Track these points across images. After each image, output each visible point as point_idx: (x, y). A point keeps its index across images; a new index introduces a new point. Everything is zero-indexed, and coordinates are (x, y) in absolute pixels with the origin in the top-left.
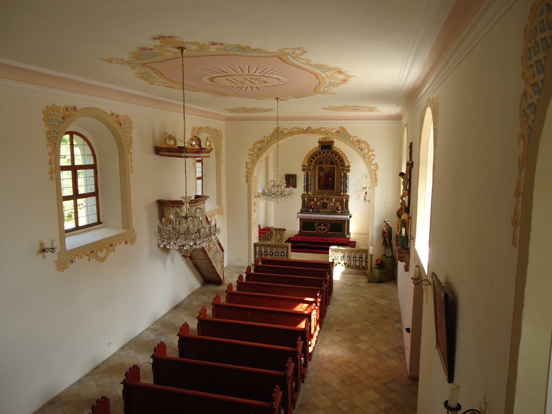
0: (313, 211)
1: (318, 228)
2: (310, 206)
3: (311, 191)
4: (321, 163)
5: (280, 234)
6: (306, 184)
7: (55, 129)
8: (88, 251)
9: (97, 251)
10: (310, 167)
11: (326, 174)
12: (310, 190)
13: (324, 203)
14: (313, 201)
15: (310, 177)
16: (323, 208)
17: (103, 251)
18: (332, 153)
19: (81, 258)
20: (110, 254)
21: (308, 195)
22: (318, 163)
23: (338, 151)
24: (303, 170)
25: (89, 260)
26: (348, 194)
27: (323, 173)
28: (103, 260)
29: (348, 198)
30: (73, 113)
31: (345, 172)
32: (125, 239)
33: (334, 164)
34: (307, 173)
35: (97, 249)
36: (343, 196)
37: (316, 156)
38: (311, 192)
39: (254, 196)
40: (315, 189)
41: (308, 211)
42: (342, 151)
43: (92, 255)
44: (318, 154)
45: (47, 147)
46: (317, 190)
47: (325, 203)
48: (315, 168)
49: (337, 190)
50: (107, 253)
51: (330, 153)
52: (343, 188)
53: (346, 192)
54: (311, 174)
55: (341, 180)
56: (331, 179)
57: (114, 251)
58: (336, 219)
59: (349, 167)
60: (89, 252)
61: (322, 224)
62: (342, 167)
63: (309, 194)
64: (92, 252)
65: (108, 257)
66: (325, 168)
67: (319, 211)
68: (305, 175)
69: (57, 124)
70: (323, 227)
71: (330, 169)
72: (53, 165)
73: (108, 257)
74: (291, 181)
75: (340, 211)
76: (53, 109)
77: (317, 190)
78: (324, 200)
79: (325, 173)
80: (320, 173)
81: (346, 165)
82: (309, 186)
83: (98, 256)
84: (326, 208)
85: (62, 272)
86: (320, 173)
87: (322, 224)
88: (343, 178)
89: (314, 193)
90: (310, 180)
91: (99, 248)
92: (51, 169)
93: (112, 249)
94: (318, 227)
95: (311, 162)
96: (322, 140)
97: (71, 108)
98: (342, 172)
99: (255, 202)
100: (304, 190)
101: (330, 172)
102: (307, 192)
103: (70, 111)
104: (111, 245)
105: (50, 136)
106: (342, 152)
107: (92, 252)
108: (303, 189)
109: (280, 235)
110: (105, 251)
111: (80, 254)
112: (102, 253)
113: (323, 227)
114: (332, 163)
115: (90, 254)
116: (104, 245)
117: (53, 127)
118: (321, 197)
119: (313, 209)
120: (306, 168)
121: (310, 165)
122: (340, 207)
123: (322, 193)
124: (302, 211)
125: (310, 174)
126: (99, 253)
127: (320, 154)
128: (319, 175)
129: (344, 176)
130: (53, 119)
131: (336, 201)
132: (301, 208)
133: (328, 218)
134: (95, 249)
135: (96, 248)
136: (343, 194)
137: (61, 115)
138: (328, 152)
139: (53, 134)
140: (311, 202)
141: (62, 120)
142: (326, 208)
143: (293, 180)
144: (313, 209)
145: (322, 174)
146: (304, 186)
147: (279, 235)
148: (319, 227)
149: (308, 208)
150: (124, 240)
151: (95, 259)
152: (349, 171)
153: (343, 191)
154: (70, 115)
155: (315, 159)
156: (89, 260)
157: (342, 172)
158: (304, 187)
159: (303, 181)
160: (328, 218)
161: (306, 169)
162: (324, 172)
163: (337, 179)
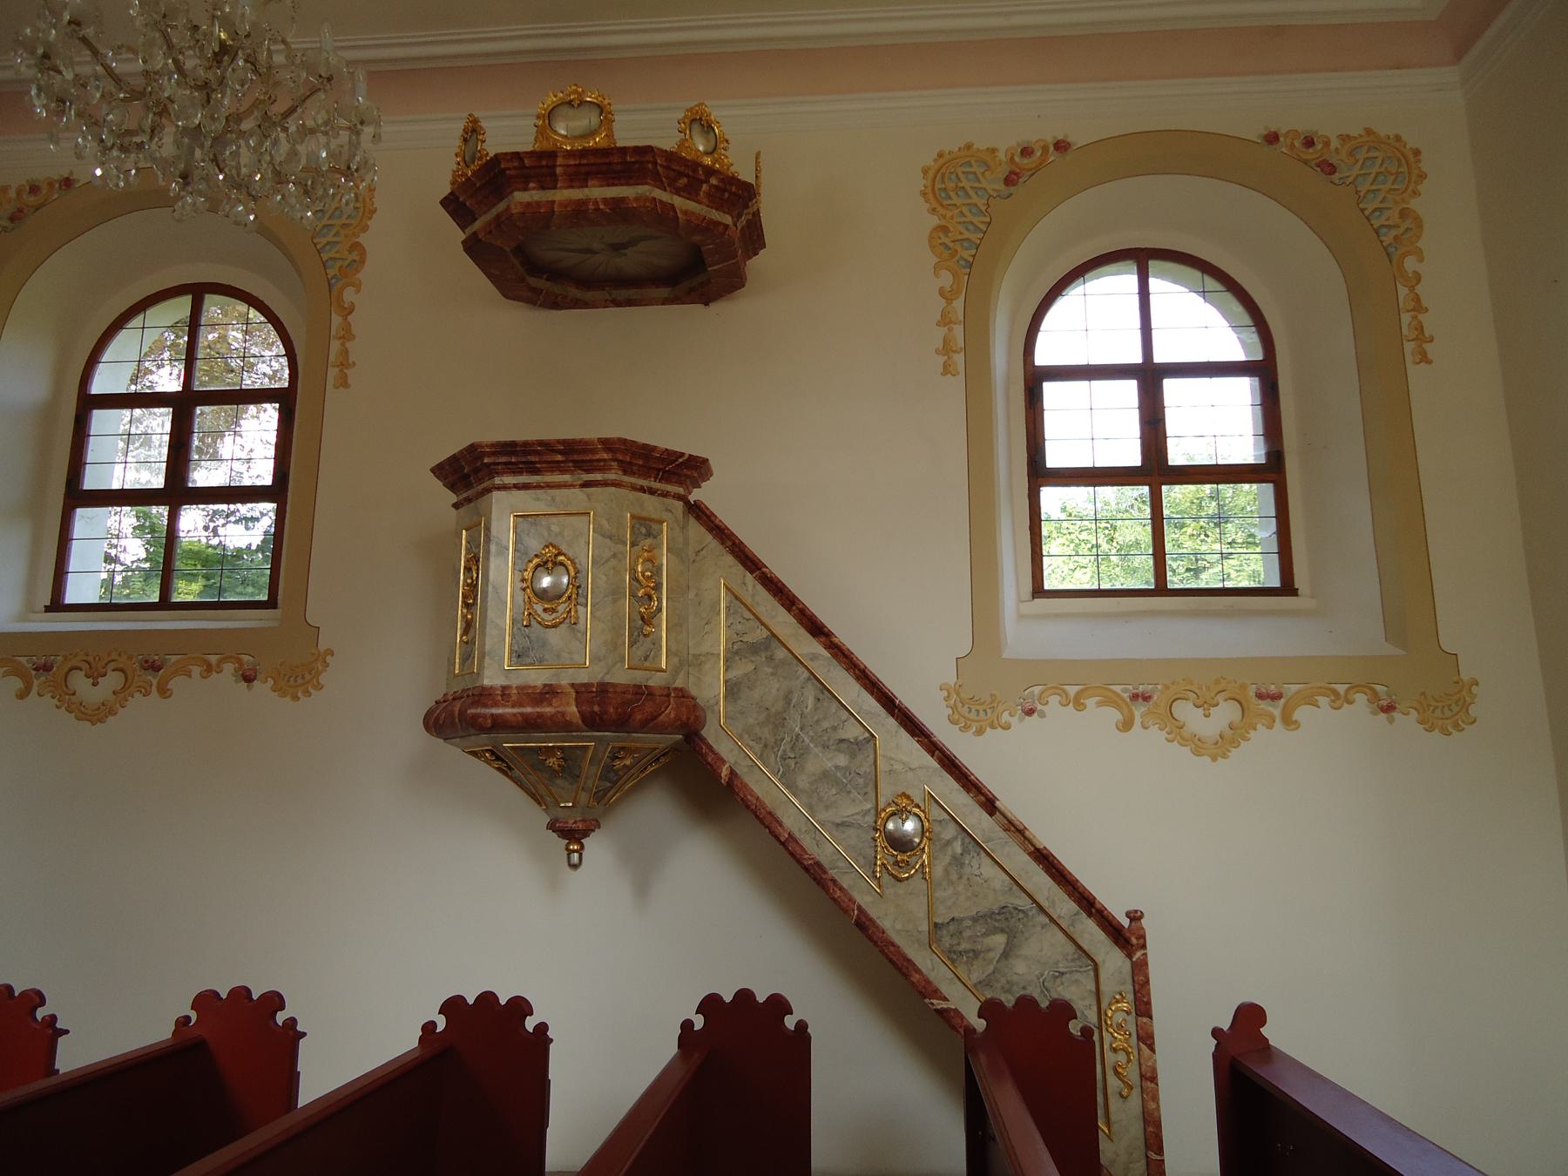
7: (970, 218)
8: (1117, 689)
9: (71, 670)
17: (100, 679)
19: (1079, 705)
20: (137, 703)
25: (22, 695)
28: (97, 714)
30: (56, 196)
32: (245, 658)
35: (74, 663)
43: (43, 678)
45: (936, 274)
50: (122, 694)
56: (256, 176)
57: (164, 692)
60: (1126, 696)
64: (47, 668)
65: (121, 710)
69: (981, 203)
72: (958, 330)
73: (121, 710)
76: (968, 159)
83: (74, 694)
85: (1166, 739)
91: (87, 662)
92: (946, 341)
93: (155, 682)
97: (51, 184)
103: (44, 192)
104: (155, 668)
105: (947, 241)
107: (47, 668)
110: (112, 681)
111: (1072, 690)
112: (94, 684)
115: (34, 672)
116: (115, 655)
117: (961, 212)
126: (80, 682)
130: (963, 188)
134: (59, 658)
135: (65, 658)
137: (1003, 172)
139: (337, 252)
141: (1001, 186)
150: (240, 661)
151: (53, 697)
154: (45, 205)
156: (22, 695)
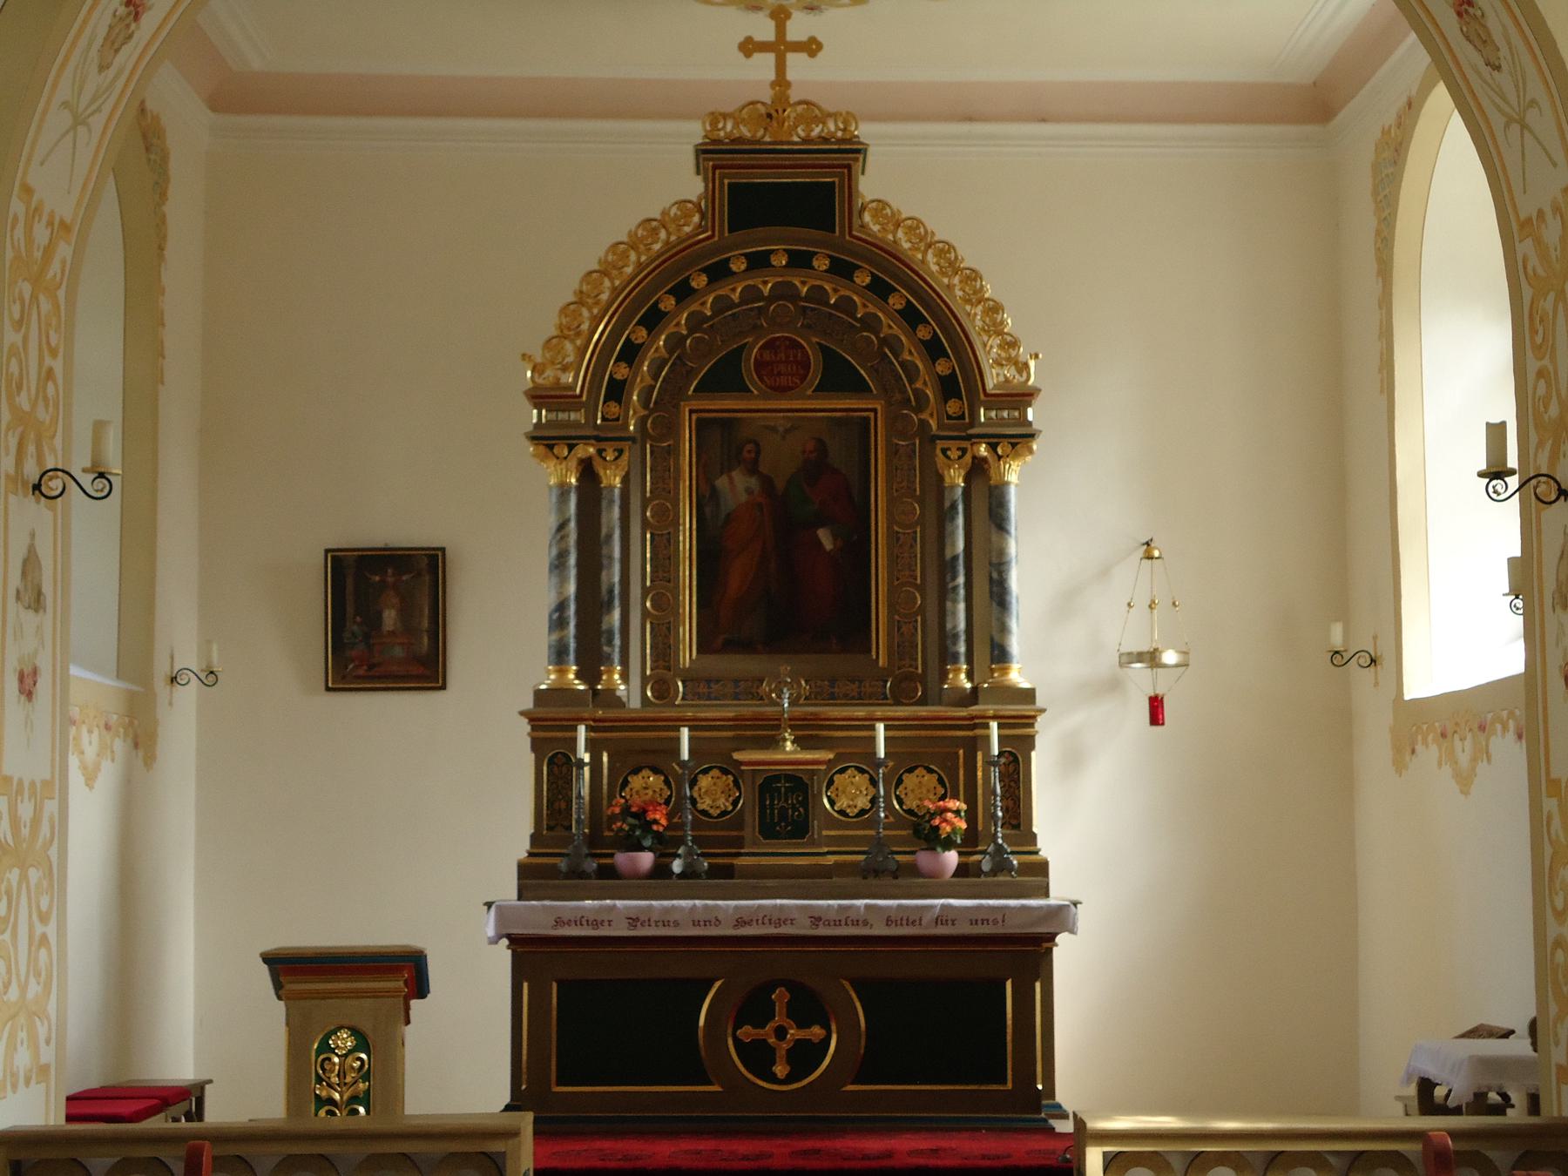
0: (661, 871)
1: (736, 1040)
2: (626, 811)
3: (625, 662)
4: (725, 378)
5: (366, 1027)
6: (572, 588)
10: (614, 408)
11: (780, 485)
12: (616, 657)
13: (776, 778)
14: (656, 770)
15: (616, 512)
16: (768, 831)
18: (842, 270)
21: (596, 705)
22: (690, 373)
23: (906, 245)
24: (545, 439)
26: (1017, 676)
27: (753, 482)
29: (1029, 721)
31: (983, 450)
33: (860, 387)
34: (588, 472)
36: (974, 696)
37: (683, 292)
38: (625, 677)
39: (32, 471)
40: (664, 650)
41: (608, 872)
42: (951, 247)
44: (700, 281)
46: (687, 654)
47: (790, 777)
48: (670, 428)
49: (902, 649)
51: (821, 264)
52: (962, 625)
53: (1000, 655)
54: (626, 480)
55: (942, 537)
56: (835, 537)
58: (938, 921)
59: (1021, 398)
61: (780, 996)
62: (952, 407)
63: (611, 691)
66: (774, 429)
67: (727, 872)
68: (563, 490)
70: (793, 1033)
71: (820, 441)
74: (390, 618)
75: (952, 858)
77: (687, 654)
78: (774, 742)
79: (767, 483)
80: (722, 483)
81: (993, 378)
82: (609, 606)
84: (800, 830)
86: (722, 483)
87: (780, 996)
88: (960, 520)
89: (663, 690)
90: (617, 553)
94: (736, 1028)
95: (653, 319)
96: (745, 131)
98: (954, 454)
99: (32, 550)
100: (559, 655)
101: (816, 466)
102: (589, 672)
106: (941, 254)
108: (541, 639)
109: (363, 1043)
113: (793, 1033)
114: (839, 378)
118: (738, 723)
119: (665, 846)
120: (577, 416)
121: (617, 391)
122: (957, 812)
123: (748, 689)
124: (532, 878)
125: (613, 479)
127: (719, 272)
128: (706, 502)
129: (967, 492)
131: (906, 758)
132: (520, 847)
133: (856, 923)
136: (970, 676)
138: (800, 261)
140: (636, 782)
142: (800, 830)
143: (406, 612)
144: (665, 846)
145: (737, 487)
146: (561, 607)
147: (345, 1040)
148: (747, 1032)
149: (594, 840)
152: (1020, 439)
153: (962, 648)
155: (695, 307)
157: (954, 454)
158: (559, 623)
159: (543, 555)
160: (856, 923)
161: (577, 425)
162: (753, 469)
163: (893, 537)
